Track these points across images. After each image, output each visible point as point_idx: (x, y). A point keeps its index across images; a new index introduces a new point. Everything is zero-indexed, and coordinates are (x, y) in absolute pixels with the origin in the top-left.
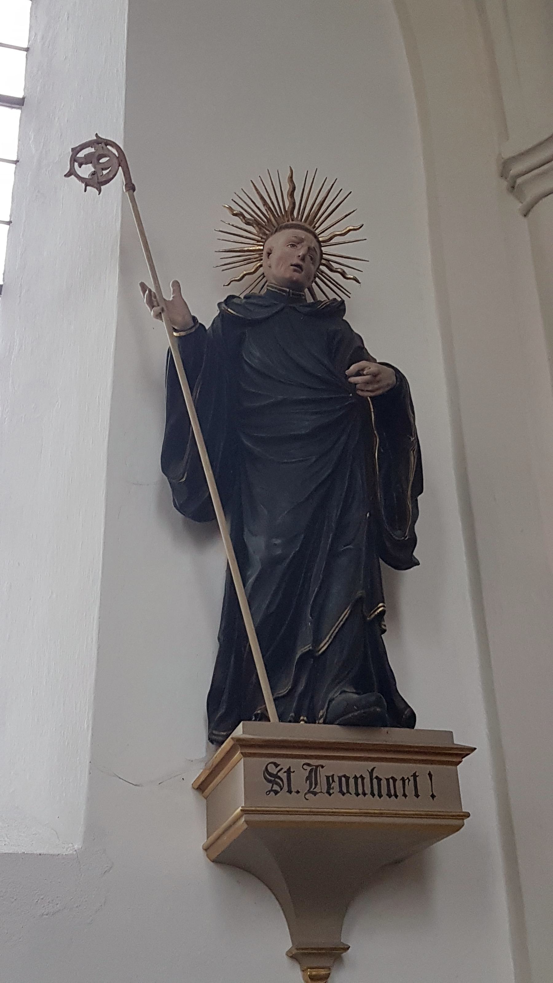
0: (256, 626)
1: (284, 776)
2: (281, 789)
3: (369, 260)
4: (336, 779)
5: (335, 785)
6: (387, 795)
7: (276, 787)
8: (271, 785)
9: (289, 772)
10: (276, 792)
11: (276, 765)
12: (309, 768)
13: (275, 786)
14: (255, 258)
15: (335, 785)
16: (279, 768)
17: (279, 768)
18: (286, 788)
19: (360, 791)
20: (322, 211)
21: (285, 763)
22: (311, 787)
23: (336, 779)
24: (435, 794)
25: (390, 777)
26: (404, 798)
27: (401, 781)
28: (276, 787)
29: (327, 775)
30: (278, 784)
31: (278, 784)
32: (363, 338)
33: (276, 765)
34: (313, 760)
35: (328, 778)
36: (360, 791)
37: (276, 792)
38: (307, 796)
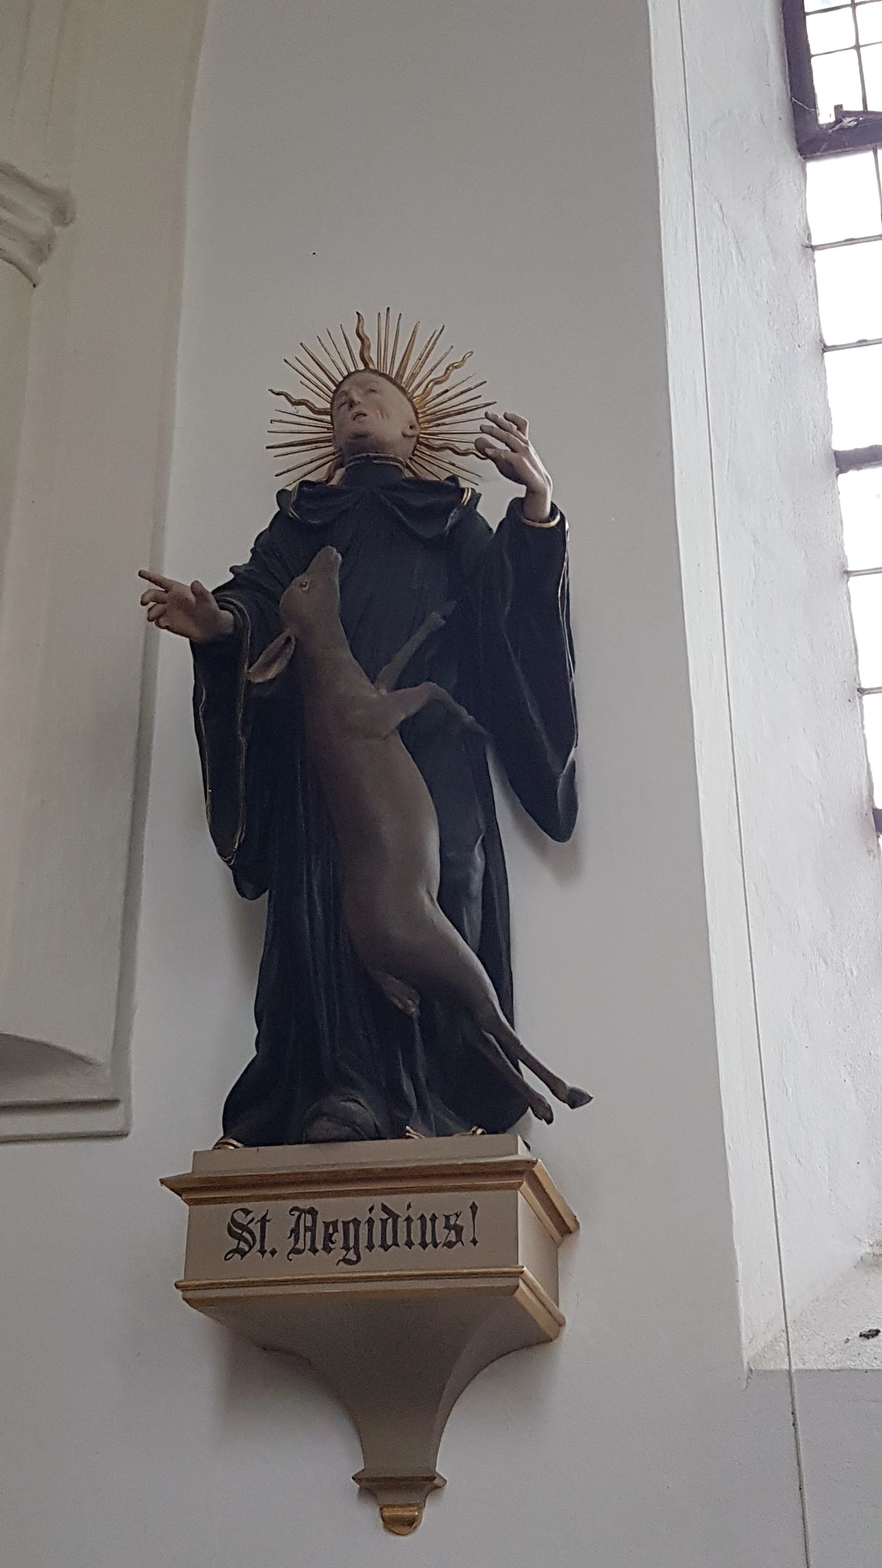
0: (477, 947)
1: (256, 1228)
2: (251, 1248)
3: (486, 380)
4: (340, 1226)
5: (338, 1237)
6: (406, 1244)
7: (243, 1245)
8: (237, 1241)
9: (264, 1220)
10: (243, 1254)
11: (247, 1212)
12: (297, 1213)
13: (242, 1243)
14: (444, 424)
15: (338, 1237)
16: (250, 1217)
17: (250, 1217)
18: (257, 1246)
19: (428, 1239)
20: (417, 383)
21: (258, 1209)
22: (296, 1242)
23: (340, 1226)
24: (477, 1239)
25: (351, 1218)
26: (421, 1248)
27: (419, 1221)
28: (243, 1245)
29: (446, 1214)
30: (246, 1241)
31: (246, 1241)
32: (502, 476)
33: (247, 1212)
34: (251, 1203)
35: (327, 1225)
36: (428, 1239)
37: (243, 1254)
38: (291, 1257)
